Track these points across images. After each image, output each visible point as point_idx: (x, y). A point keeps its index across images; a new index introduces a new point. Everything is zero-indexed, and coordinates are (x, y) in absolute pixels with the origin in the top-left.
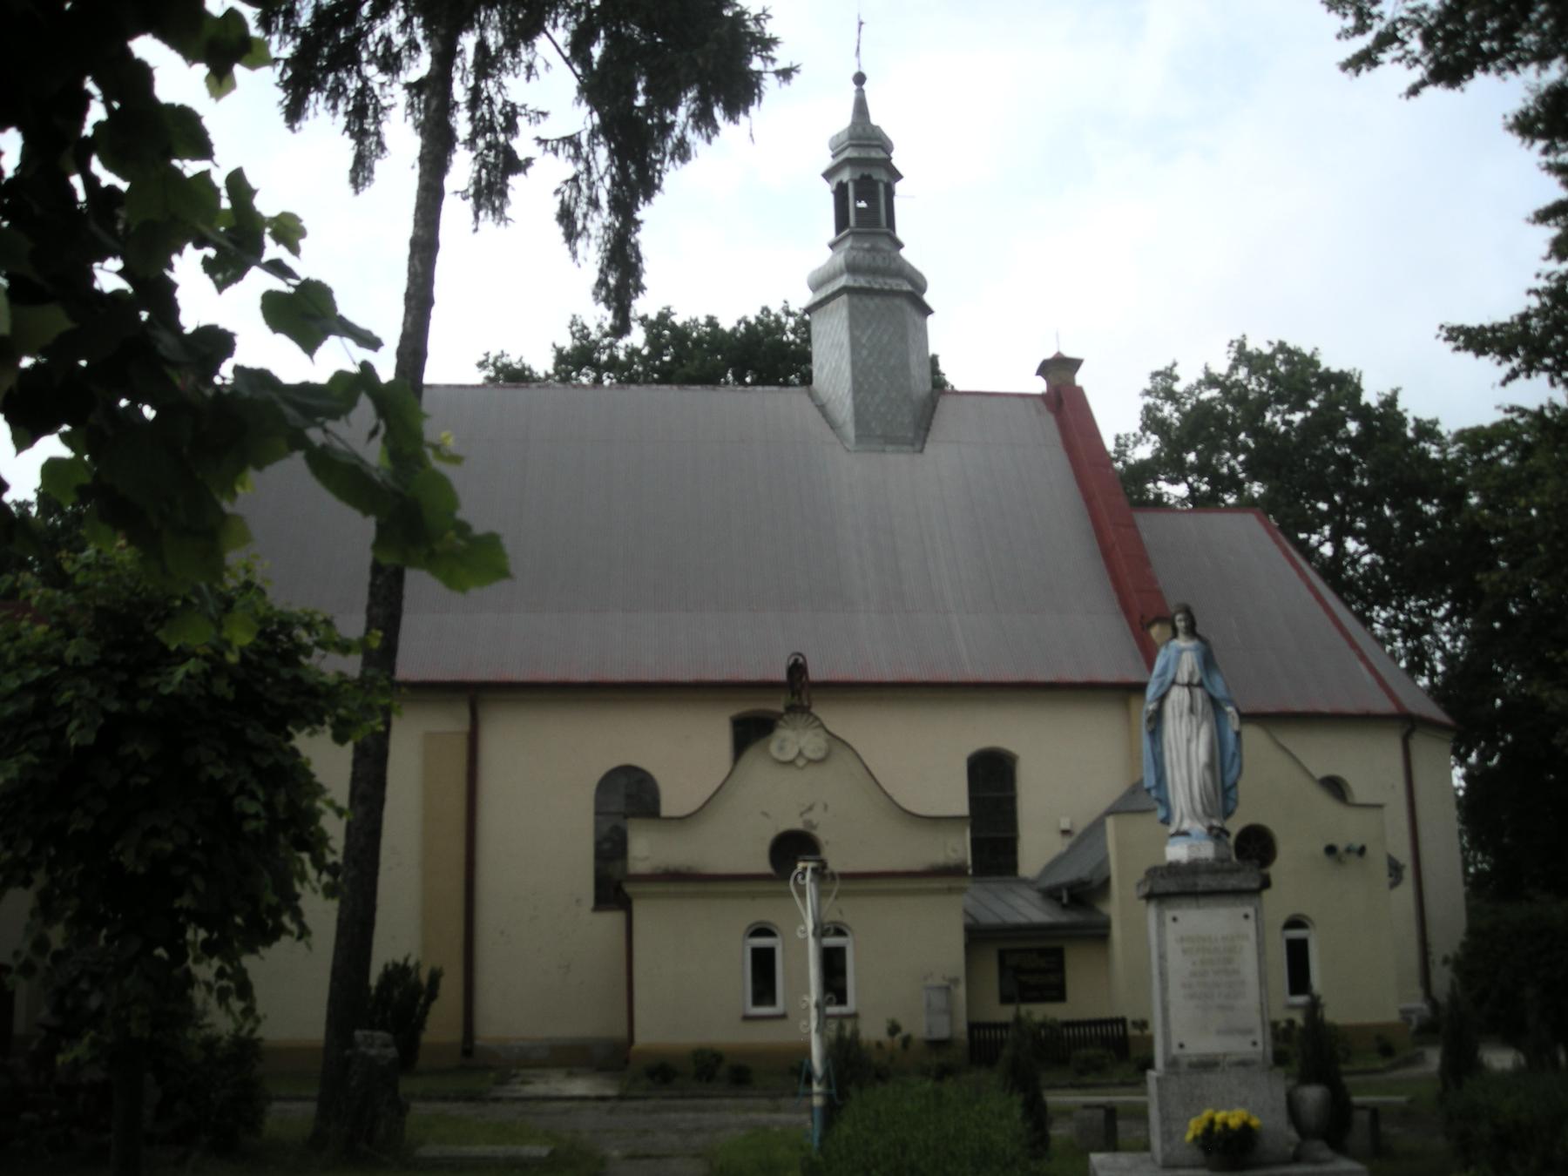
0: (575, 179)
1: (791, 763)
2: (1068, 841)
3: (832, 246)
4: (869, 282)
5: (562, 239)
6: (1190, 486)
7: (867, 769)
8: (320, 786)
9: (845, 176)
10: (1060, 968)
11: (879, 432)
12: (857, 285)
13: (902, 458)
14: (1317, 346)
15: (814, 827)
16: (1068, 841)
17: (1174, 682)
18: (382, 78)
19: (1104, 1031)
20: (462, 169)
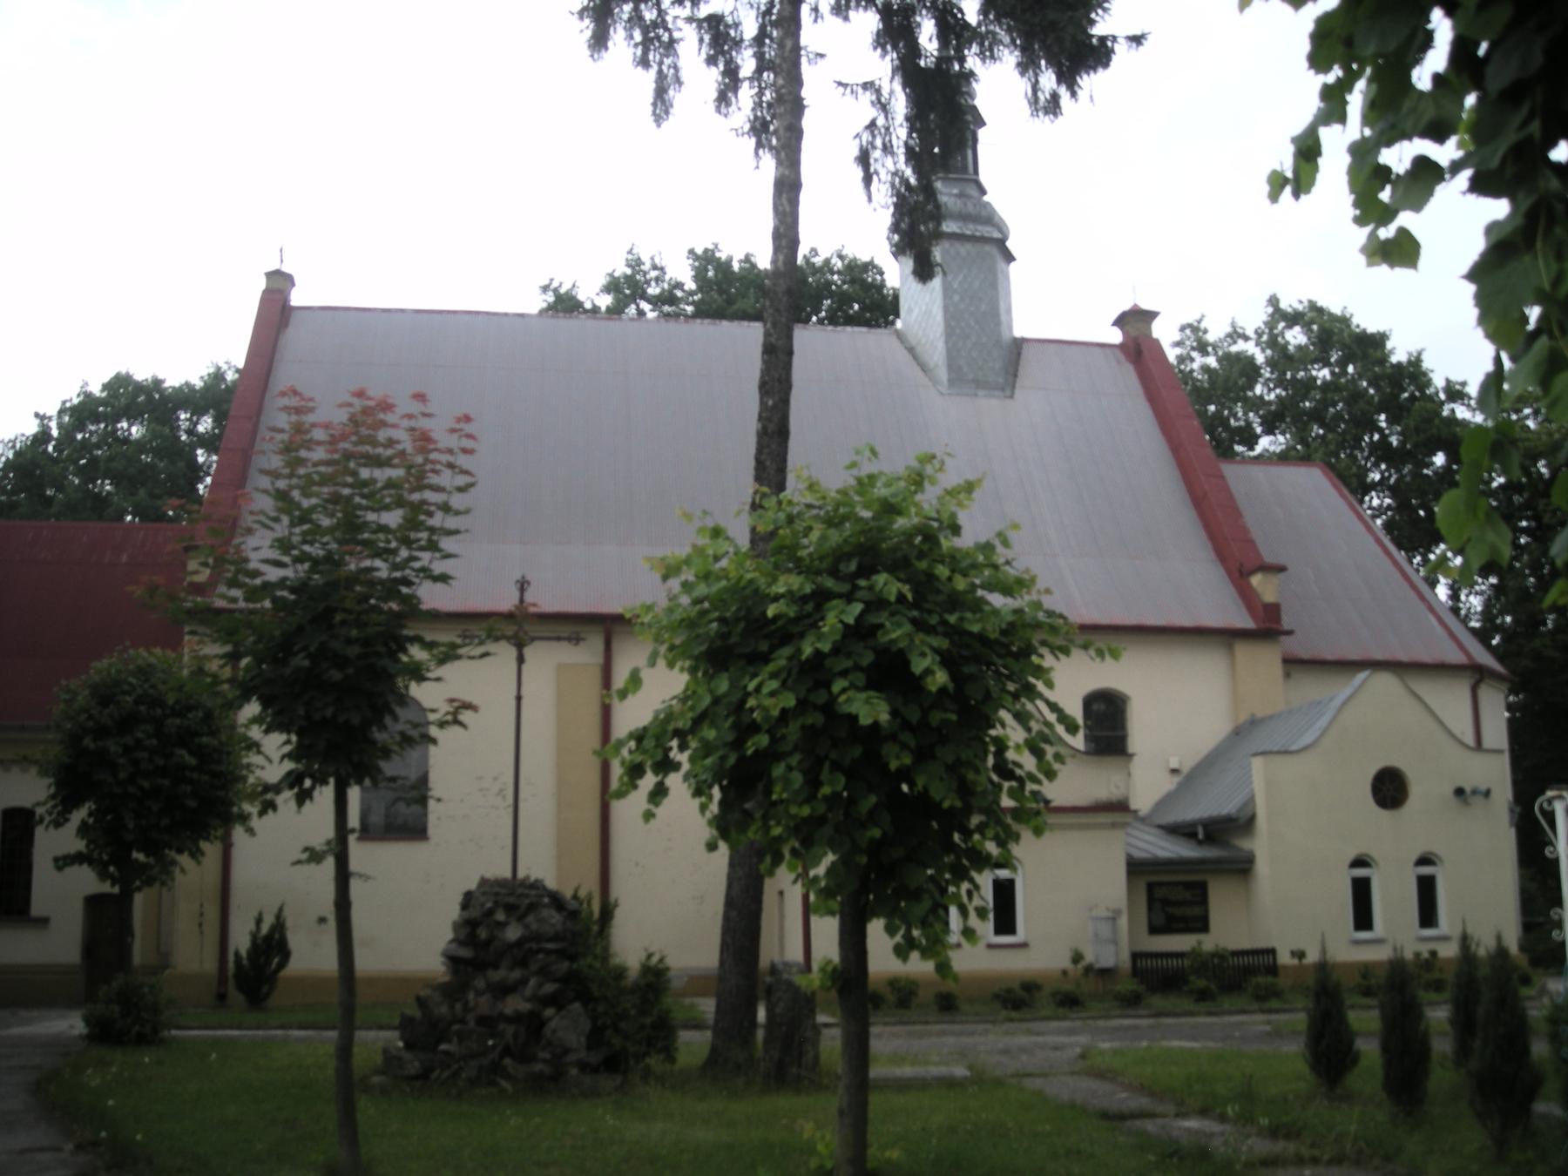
2: (1176, 779)
4: (960, 228)
7: (519, 698)
10: (1204, 901)
11: (971, 377)
13: (994, 402)
14: (1345, 305)
16: (1176, 779)
19: (1251, 961)
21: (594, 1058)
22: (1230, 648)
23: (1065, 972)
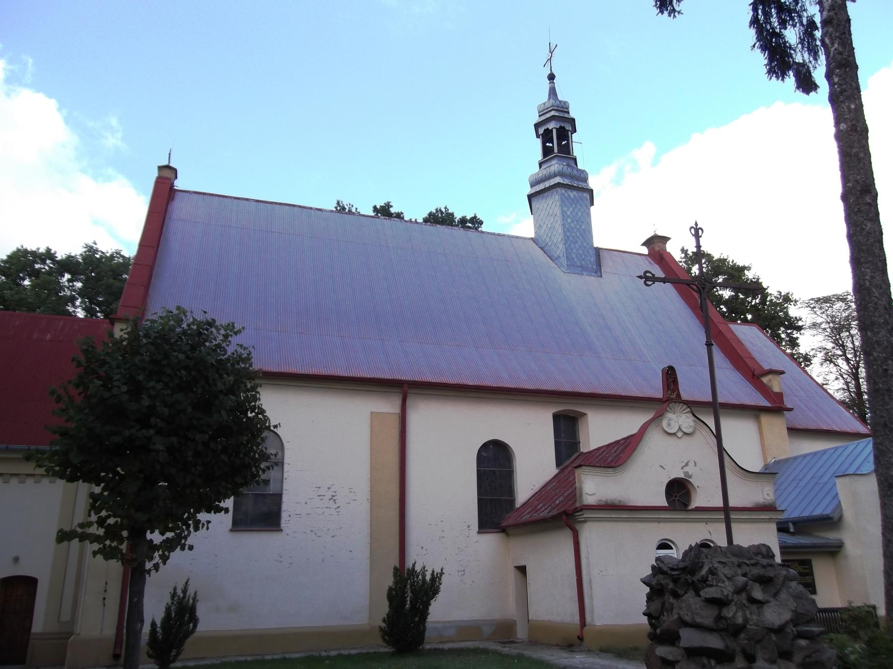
1: (674, 434)
8: (85, 482)
9: (552, 125)
15: (690, 477)
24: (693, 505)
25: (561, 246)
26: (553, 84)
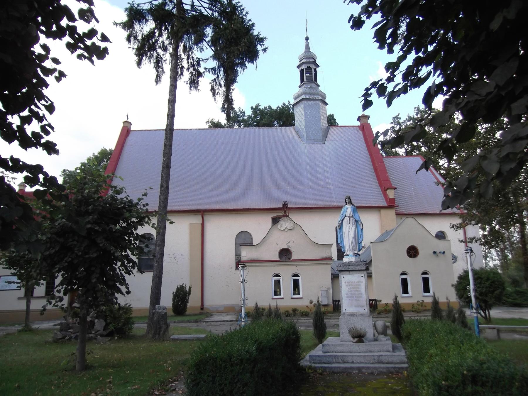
0: (215, 79)
3: (300, 87)
4: (309, 97)
5: (212, 95)
6: (406, 149)
9: (303, 67)
12: (306, 98)
13: (319, 145)
15: (290, 247)
17: (345, 216)
18: (162, 53)
20: (187, 75)
21: (105, 333)
22: (380, 211)
23: (307, 307)
24: (292, 259)
25: (304, 130)
26: (307, 43)
